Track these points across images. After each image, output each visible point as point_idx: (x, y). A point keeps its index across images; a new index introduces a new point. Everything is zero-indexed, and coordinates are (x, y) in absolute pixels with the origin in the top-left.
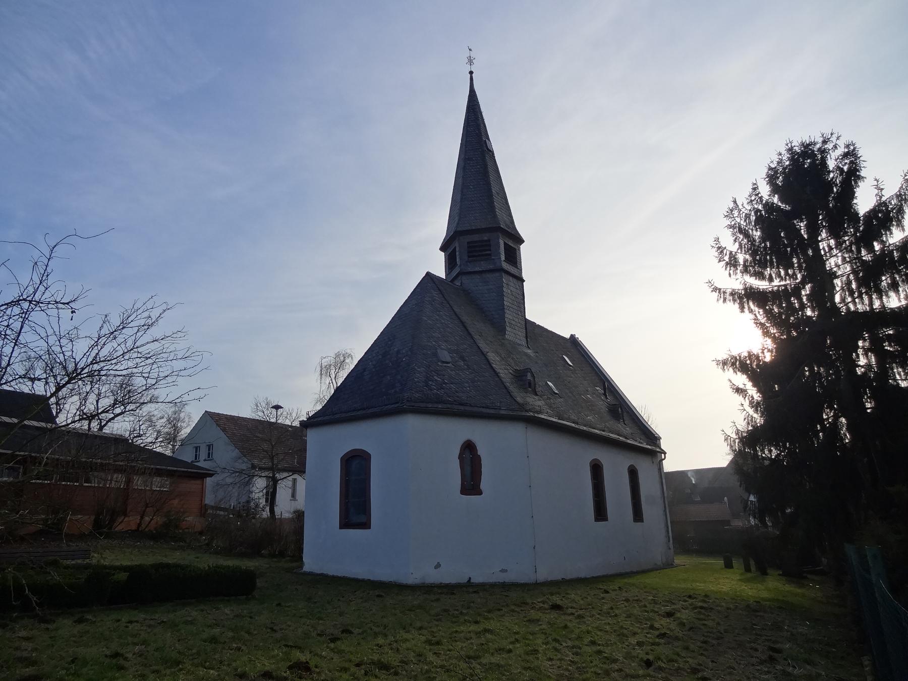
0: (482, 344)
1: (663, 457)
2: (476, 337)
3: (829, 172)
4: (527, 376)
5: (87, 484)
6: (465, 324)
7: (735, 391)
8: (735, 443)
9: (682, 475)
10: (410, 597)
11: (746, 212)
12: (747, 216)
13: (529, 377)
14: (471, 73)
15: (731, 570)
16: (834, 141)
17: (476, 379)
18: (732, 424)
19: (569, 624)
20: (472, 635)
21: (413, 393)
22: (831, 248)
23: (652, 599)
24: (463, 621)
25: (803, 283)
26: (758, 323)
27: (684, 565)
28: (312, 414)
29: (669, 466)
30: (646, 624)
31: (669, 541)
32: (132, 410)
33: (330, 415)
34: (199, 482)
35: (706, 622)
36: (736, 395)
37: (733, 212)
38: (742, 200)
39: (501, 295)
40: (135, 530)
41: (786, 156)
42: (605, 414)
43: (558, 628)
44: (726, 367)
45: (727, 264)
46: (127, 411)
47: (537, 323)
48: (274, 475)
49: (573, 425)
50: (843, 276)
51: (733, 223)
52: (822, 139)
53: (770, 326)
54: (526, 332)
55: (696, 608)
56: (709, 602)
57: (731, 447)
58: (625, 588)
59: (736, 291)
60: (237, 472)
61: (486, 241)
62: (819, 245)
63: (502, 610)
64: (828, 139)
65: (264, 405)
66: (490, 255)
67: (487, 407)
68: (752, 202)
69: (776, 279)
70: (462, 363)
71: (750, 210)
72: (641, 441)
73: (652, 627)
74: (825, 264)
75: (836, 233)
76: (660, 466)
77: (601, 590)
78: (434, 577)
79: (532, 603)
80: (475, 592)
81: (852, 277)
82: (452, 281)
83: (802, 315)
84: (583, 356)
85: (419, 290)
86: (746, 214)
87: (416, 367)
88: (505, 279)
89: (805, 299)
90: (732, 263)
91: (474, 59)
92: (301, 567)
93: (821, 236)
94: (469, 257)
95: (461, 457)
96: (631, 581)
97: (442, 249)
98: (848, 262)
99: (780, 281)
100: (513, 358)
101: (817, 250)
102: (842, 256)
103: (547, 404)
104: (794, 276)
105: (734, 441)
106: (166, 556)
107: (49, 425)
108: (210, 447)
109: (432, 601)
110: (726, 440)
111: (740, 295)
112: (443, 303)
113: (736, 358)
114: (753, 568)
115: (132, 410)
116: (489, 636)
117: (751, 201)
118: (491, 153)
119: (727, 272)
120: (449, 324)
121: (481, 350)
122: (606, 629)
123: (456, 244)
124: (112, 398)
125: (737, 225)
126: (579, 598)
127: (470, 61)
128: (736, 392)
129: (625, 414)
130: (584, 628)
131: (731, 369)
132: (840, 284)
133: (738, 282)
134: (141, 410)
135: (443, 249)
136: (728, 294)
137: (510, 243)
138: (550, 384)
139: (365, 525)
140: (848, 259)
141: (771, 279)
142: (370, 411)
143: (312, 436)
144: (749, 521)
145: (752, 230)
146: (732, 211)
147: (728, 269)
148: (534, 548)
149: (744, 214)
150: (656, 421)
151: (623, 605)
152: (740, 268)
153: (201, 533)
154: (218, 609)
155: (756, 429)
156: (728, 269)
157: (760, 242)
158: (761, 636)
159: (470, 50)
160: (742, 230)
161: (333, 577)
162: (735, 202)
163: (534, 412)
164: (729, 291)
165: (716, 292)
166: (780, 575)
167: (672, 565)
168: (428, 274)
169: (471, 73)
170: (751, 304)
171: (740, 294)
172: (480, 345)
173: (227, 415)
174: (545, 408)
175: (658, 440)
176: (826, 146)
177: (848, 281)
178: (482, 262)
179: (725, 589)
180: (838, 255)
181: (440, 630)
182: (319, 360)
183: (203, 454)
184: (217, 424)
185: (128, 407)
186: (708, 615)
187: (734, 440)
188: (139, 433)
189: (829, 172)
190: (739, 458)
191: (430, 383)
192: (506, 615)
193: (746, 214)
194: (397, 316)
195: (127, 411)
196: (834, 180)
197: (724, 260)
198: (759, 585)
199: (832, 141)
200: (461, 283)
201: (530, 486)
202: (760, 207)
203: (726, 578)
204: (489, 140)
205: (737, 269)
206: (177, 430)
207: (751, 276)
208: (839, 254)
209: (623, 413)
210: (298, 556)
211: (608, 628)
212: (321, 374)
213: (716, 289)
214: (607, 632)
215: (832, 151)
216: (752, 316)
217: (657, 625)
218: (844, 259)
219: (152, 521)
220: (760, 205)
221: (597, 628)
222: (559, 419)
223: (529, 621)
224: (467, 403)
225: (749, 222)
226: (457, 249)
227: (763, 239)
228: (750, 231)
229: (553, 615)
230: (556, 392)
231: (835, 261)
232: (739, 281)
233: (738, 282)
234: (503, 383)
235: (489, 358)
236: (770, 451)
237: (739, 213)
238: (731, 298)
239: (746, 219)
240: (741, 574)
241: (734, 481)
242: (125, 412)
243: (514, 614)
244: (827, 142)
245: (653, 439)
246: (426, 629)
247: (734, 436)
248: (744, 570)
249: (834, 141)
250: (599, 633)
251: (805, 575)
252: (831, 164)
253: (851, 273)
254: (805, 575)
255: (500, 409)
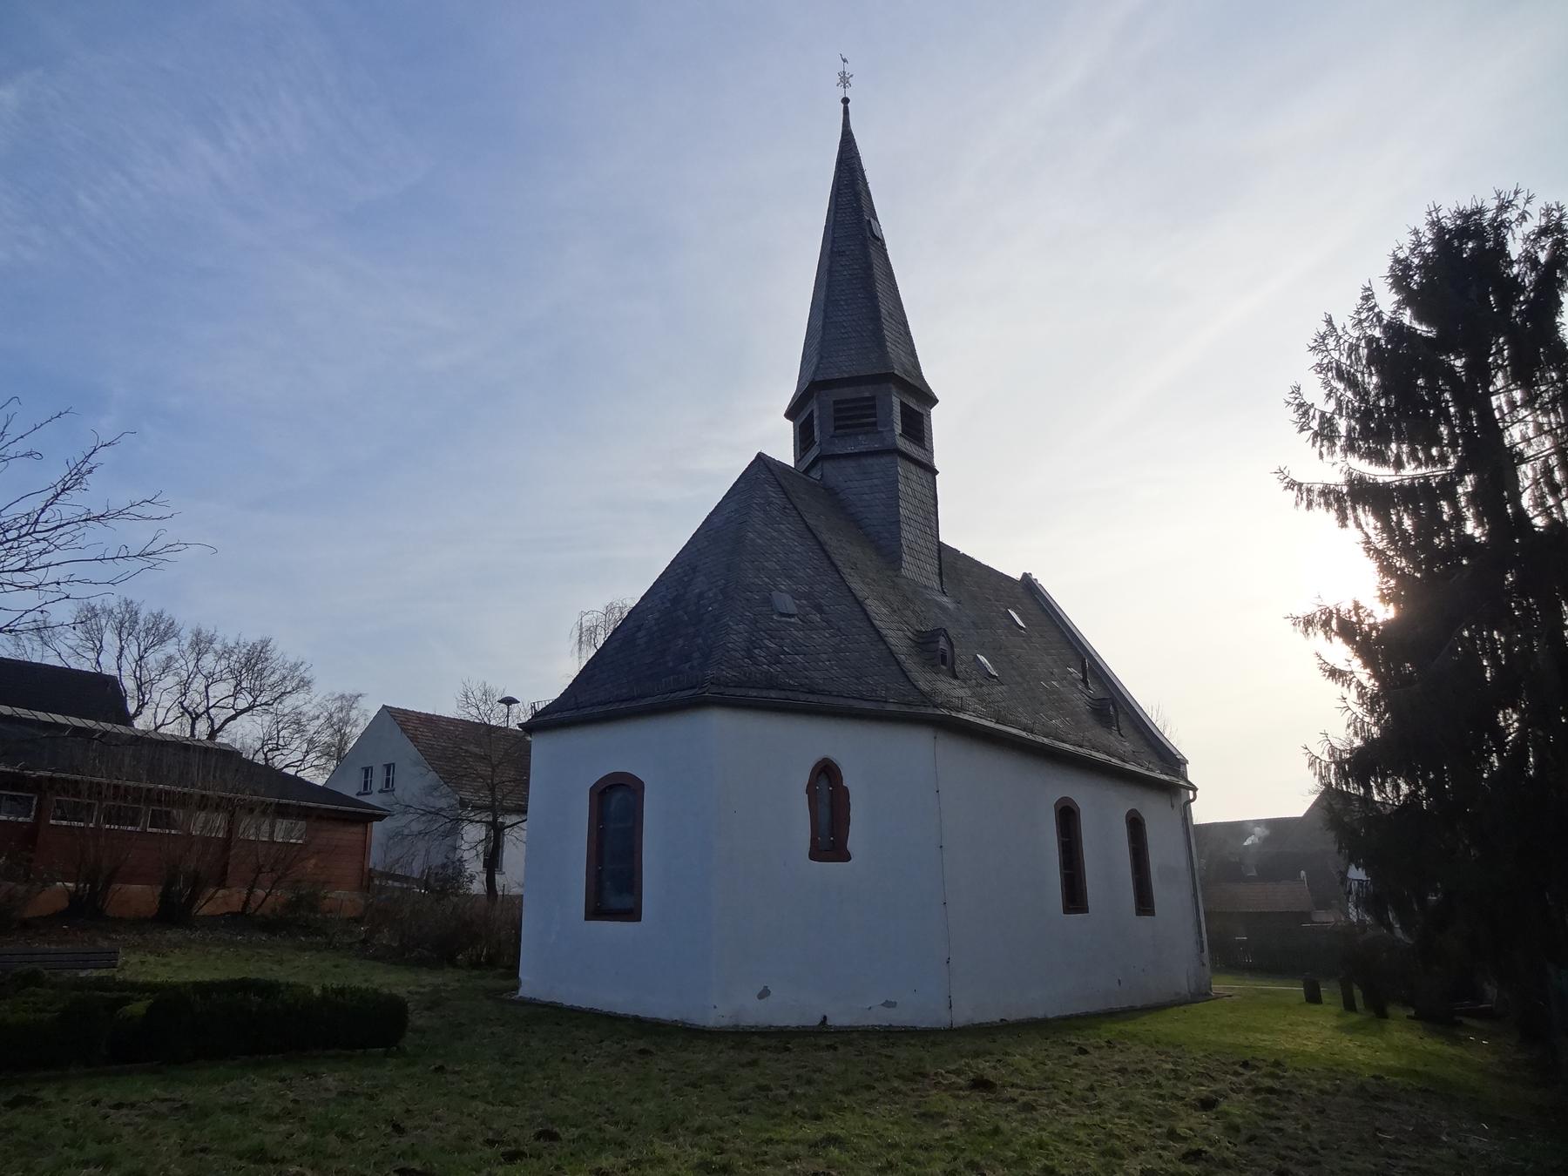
0: (856, 585)
1: (1191, 797)
2: (846, 571)
3: (1511, 263)
4: (938, 641)
5: (155, 830)
6: (827, 547)
7: (1327, 674)
8: (1329, 770)
9: (1236, 830)
10: (702, 1056)
11: (1350, 341)
12: (1354, 349)
13: (942, 644)
14: (846, 101)
15: (1318, 1007)
16: (1521, 206)
17: (843, 646)
18: (1322, 737)
19: (1004, 1125)
20: (801, 1150)
21: (723, 670)
22: (1512, 405)
23: (1173, 1070)
24: (790, 1115)
25: (1461, 471)
26: (1371, 550)
27: (1230, 996)
28: (541, 708)
29: (1204, 812)
30: (1160, 1127)
31: (1202, 951)
32: (266, 704)
33: (572, 709)
34: (358, 829)
35: (1280, 1124)
36: (1330, 683)
37: (1326, 342)
38: (1343, 320)
39: (894, 497)
40: (238, 913)
41: (1428, 235)
42: (1084, 717)
43: (981, 1134)
44: (1310, 629)
45: (1316, 434)
46: (258, 706)
47: (962, 551)
48: (495, 819)
49: (1024, 734)
50: (1538, 459)
51: (1326, 361)
52: (1496, 203)
53: (1394, 555)
54: (940, 565)
55: (1256, 1091)
56: (1283, 1077)
57: (1322, 777)
58: (1120, 1043)
59: (1332, 487)
60: (430, 813)
61: (867, 399)
62: (1490, 402)
63: (874, 1088)
64: (1510, 202)
65: (478, 694)
66: (875, 424)
67: (862, 698)
68: (1362, 324)
69: (1409, 464)
70: (817, 618)
71: (1358, 338)
72: (1150, 766)
73: (1172, 1135)
74: (1502, 438)
75: (1523, 375)
76: (1185, 814)
77: (1073, 1048)
78: (757, 1014)
79: (936, 1074)
80: (829, 1047)
81: (1553, 461)
82: (806, 471)
83: (1457, 535)
84: (1044, 610)
85: (743, 485)
86: (1351, 344)
87: (731, 623)
88: (902, 468)
89: (1463, 501)
90: (1326, 432)
91: (852, 76)
92: (517, 988)
93: (1494, 384)
94: (836, 428)
95: (811, 790)
96: (1130, 1027)
97: (789, 415)
98: (1545, 432)
99: (1416, 468)
100: (914, 611)
101: (1486, 411)
102: (1535, 421)
103: (974, 695)
104: (1443, 460)
105: (1327, 767)
106: (280, 963)
107: (122, 729)
108: (389, 768)
109: (743, 1066)
110: (1311, 764)
111: (1338, 495)
112: (785, 508)
113: (1331, 612)
114: (1359, 1004)
115: (266, 704)
116: (834, 1152)
117: (1360, 321)
118: (880, 243)
119: (1316, 450)
120: (796, 546)
121: (854, 595)
122: (1078, 1137)
123: (814, 406)
124: (233, 682)
125: (1334, 365)
126: (1028, 1065)
127: (845, 80)
128: (1329, 676)
129: (1121, 717)
130: (1033, 1133)
131: (1321, 634)
132: (1530, 474)
133: (1334, 469)
134: (280, 703)
135: (790, 414)
136: (1316, 493)
137: (913, 404)
138: (982, 658)
139: (632, 913)
140: (1546, 428)
141: (1399, 465)
142: (649, 701)
143: (541, 747)
144: (1347, 915)
145: (1363, 373)
146: (1323, 338)
147: (1318, 444)
148: (948, 962)
149: (1347, 345)
150: (1177, 732)
151: (1114, 1082)
152: (1340, 443)
153: (358, 921)
154: (315, 1076)
155: (1370, 743)
156: (1318, 444)
157: (1377, 395)
158: (1396, 1157)
159: (845, 61)
160: (1343, 374)
161: (572, 1009)
162: (1329, 322)
163: (950, 709)
164: (1317, 488)
165: (1293, 489)
166: (1409, 1017)
167: (1207, 994)
168: (761, 457)
169: (846, 101)
170: (1360, 511)
171: (1339, 492)
172: (853, 585)
173: (420, 713)
174: (973, 703)
175: (1182, 767)
176: (1504, 216)
177: (1545, 468)
178: (860, 438)
179: (1312, 1047)
180: (1527, 419)
181: (737, 1137)
182: (577, 618)
183: (377, 782)
184: (402, 729)
185: (259, 699)
186: (1286, 1108)
187: (1328, 765)
188: (277, 744)
189: (1511, 263)
190: (1331, 802)
191: (756, 651)
192: (881, 1099)
193: (1351, 344)
194: (702, 532)
195: (258, 706)
196: (1519, 280)
197: (1310, 428)
198: (1376, 1040)
199: (1517, 206)
200: (822, 475)
201: (941, 847)
202: (1377, 333)
203: (1312, 1023)
204: (876, 219)
205: (1335, 444)
206: (343, 739)
207: (1361, 457)
208: (1530, 418)
209: (1118, 715)
210: (513, 970)
211: (1082, 1135)
212: (580, 641)
213: (1292, 485)
214: (1079, 1143)
215: (1517, 225)
216: (1360, 537)
217: (1181, 1129)
218: (1539, 428)
219: (269, 898)
220: (1378, 329)
221: (1060, 1135)
222: (997, 723)
223: (923, 1115)
224: (824, 690)
225: (1356, 359)
226: (816, 414)
227: (1384, 390)
228: (1359, 375)
229: (973, 1103)
230: (994, 673)
231: (1521, 431)
232: (1337, 468)
233: (1334, 469)
234: (891, 653)
235: (868, 609)
236: (1397, 787)
237: (1338, 342)
238: (1322, 501)
239: (1352, 353)
240: (1338, 1016)
241: (1327, 843)
242: (254, 706)
243: (896, 1098)
244: (1508, 207)
245: (1174, 763)
246: (709, 1132)
247: (1326, 757)
248: (1343, 1009)
249: (1521, 206)
250: (1062, 1147)
251: (1457, 1018)
252: (1515, 249)
253: (1552, 454)
254: (1457, 1018)
255: (886, 702)
